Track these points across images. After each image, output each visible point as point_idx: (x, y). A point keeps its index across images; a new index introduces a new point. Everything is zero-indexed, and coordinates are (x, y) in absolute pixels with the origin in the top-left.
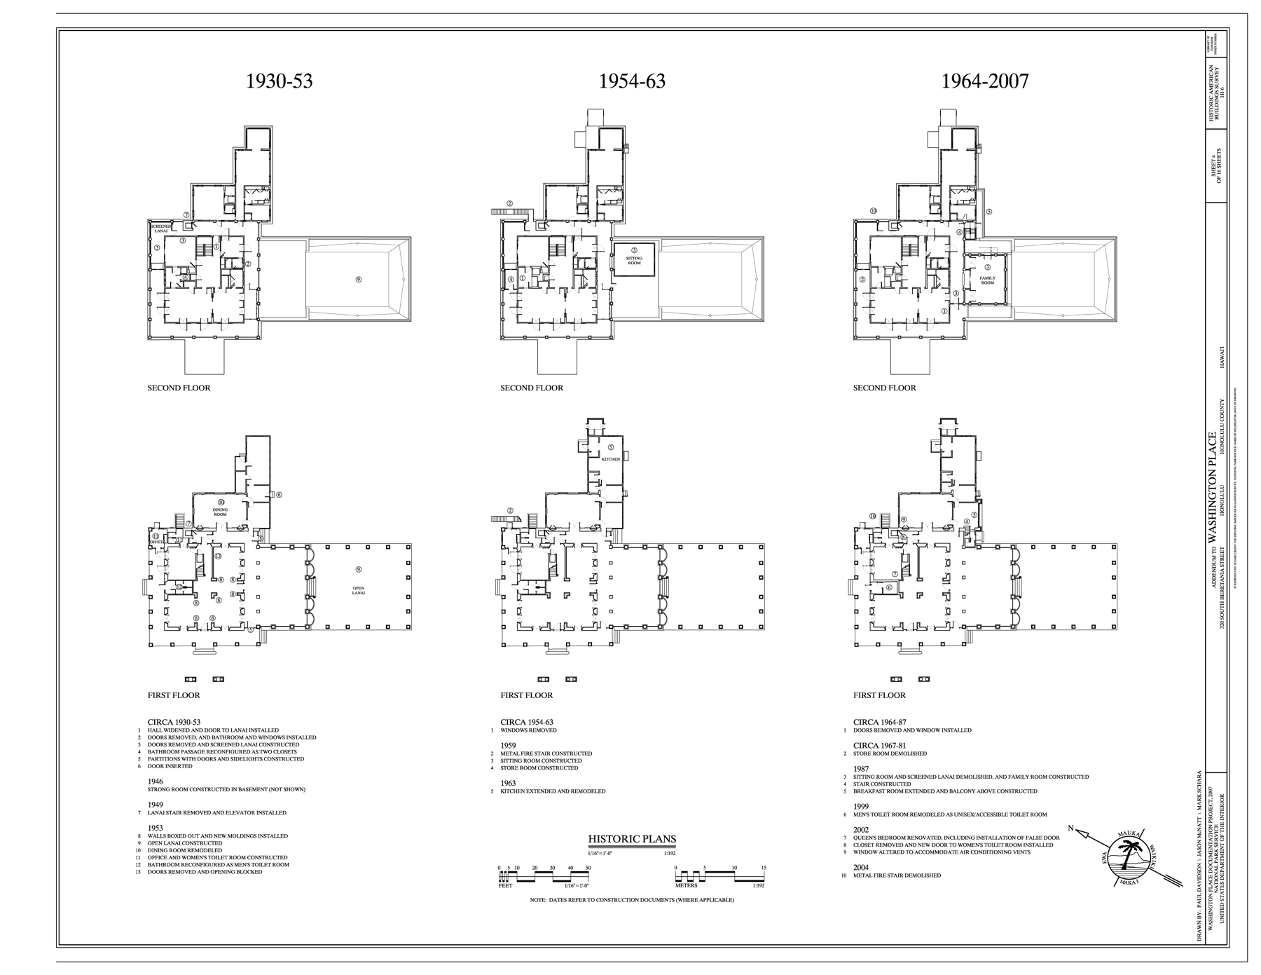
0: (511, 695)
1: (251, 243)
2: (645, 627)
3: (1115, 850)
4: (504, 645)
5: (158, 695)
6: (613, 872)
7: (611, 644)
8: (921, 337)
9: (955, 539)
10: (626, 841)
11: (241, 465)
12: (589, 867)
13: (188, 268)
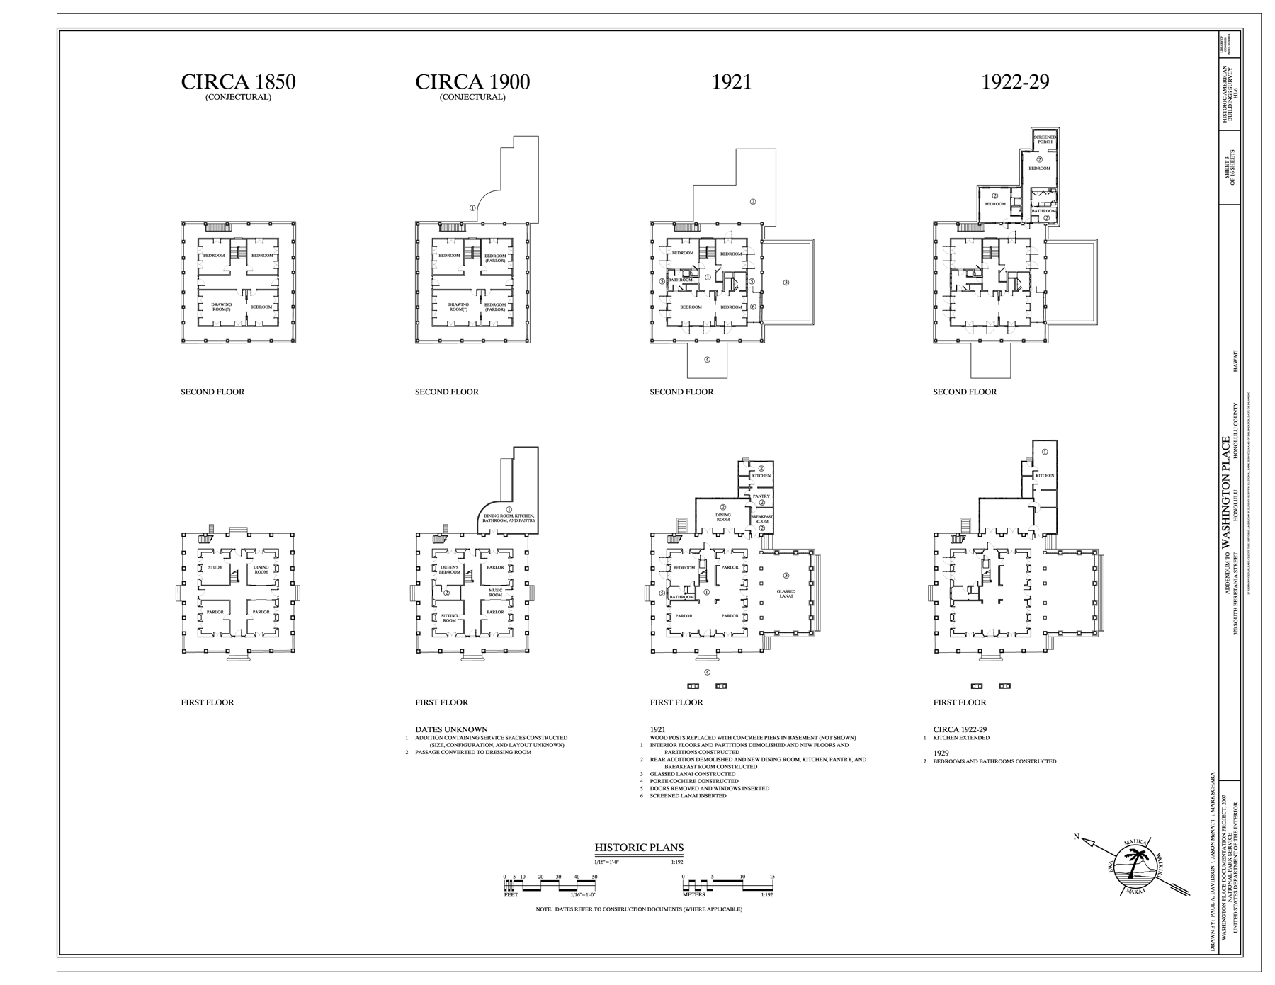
0: (192, 703)
1: (1038, 246)
2: (1079, 633)
3: (1121, 859)
4: (937, 651)
5: (660, 702)
6: (620, 881)
7: (1045, 651)
8: (1002, 341)
9: (1040, 543)
10: (633, 850)
11: (1028, 469)
12: (595, 876)
13: (690, 270)
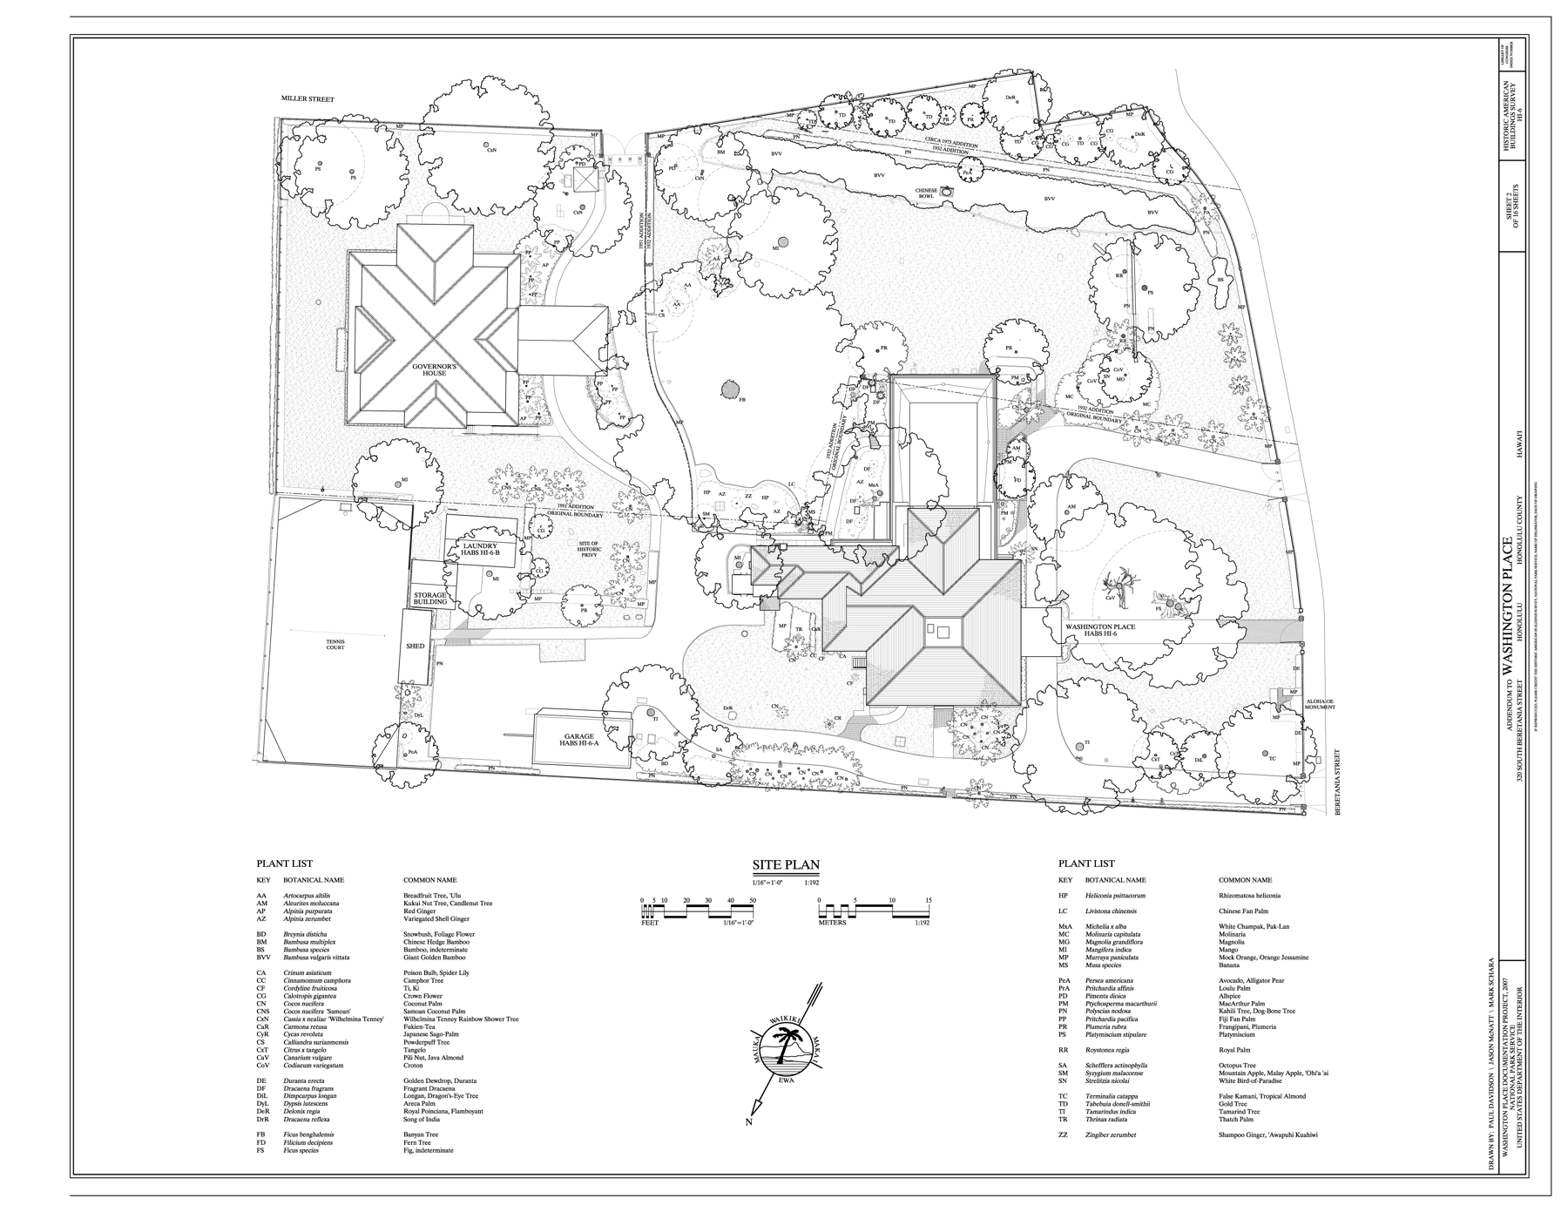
3: (769, 1040)
12: (753, 900)
